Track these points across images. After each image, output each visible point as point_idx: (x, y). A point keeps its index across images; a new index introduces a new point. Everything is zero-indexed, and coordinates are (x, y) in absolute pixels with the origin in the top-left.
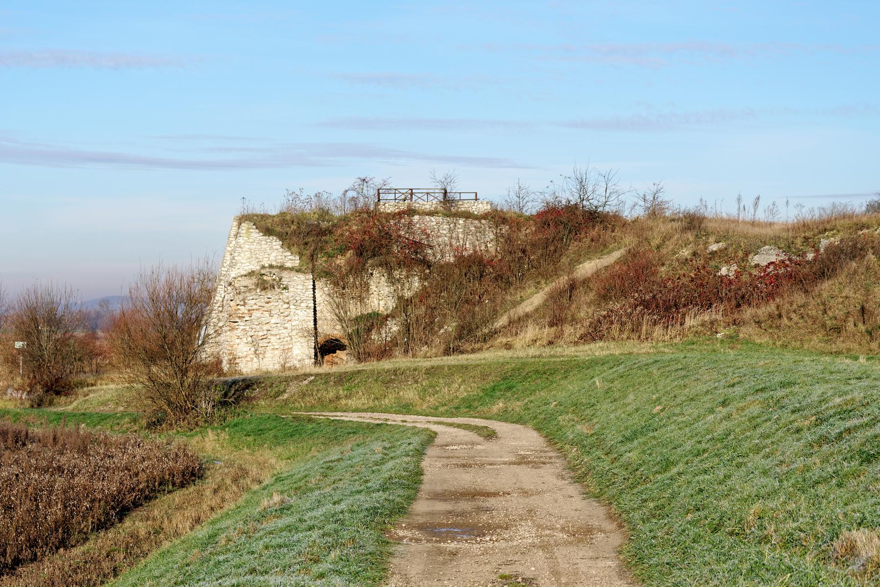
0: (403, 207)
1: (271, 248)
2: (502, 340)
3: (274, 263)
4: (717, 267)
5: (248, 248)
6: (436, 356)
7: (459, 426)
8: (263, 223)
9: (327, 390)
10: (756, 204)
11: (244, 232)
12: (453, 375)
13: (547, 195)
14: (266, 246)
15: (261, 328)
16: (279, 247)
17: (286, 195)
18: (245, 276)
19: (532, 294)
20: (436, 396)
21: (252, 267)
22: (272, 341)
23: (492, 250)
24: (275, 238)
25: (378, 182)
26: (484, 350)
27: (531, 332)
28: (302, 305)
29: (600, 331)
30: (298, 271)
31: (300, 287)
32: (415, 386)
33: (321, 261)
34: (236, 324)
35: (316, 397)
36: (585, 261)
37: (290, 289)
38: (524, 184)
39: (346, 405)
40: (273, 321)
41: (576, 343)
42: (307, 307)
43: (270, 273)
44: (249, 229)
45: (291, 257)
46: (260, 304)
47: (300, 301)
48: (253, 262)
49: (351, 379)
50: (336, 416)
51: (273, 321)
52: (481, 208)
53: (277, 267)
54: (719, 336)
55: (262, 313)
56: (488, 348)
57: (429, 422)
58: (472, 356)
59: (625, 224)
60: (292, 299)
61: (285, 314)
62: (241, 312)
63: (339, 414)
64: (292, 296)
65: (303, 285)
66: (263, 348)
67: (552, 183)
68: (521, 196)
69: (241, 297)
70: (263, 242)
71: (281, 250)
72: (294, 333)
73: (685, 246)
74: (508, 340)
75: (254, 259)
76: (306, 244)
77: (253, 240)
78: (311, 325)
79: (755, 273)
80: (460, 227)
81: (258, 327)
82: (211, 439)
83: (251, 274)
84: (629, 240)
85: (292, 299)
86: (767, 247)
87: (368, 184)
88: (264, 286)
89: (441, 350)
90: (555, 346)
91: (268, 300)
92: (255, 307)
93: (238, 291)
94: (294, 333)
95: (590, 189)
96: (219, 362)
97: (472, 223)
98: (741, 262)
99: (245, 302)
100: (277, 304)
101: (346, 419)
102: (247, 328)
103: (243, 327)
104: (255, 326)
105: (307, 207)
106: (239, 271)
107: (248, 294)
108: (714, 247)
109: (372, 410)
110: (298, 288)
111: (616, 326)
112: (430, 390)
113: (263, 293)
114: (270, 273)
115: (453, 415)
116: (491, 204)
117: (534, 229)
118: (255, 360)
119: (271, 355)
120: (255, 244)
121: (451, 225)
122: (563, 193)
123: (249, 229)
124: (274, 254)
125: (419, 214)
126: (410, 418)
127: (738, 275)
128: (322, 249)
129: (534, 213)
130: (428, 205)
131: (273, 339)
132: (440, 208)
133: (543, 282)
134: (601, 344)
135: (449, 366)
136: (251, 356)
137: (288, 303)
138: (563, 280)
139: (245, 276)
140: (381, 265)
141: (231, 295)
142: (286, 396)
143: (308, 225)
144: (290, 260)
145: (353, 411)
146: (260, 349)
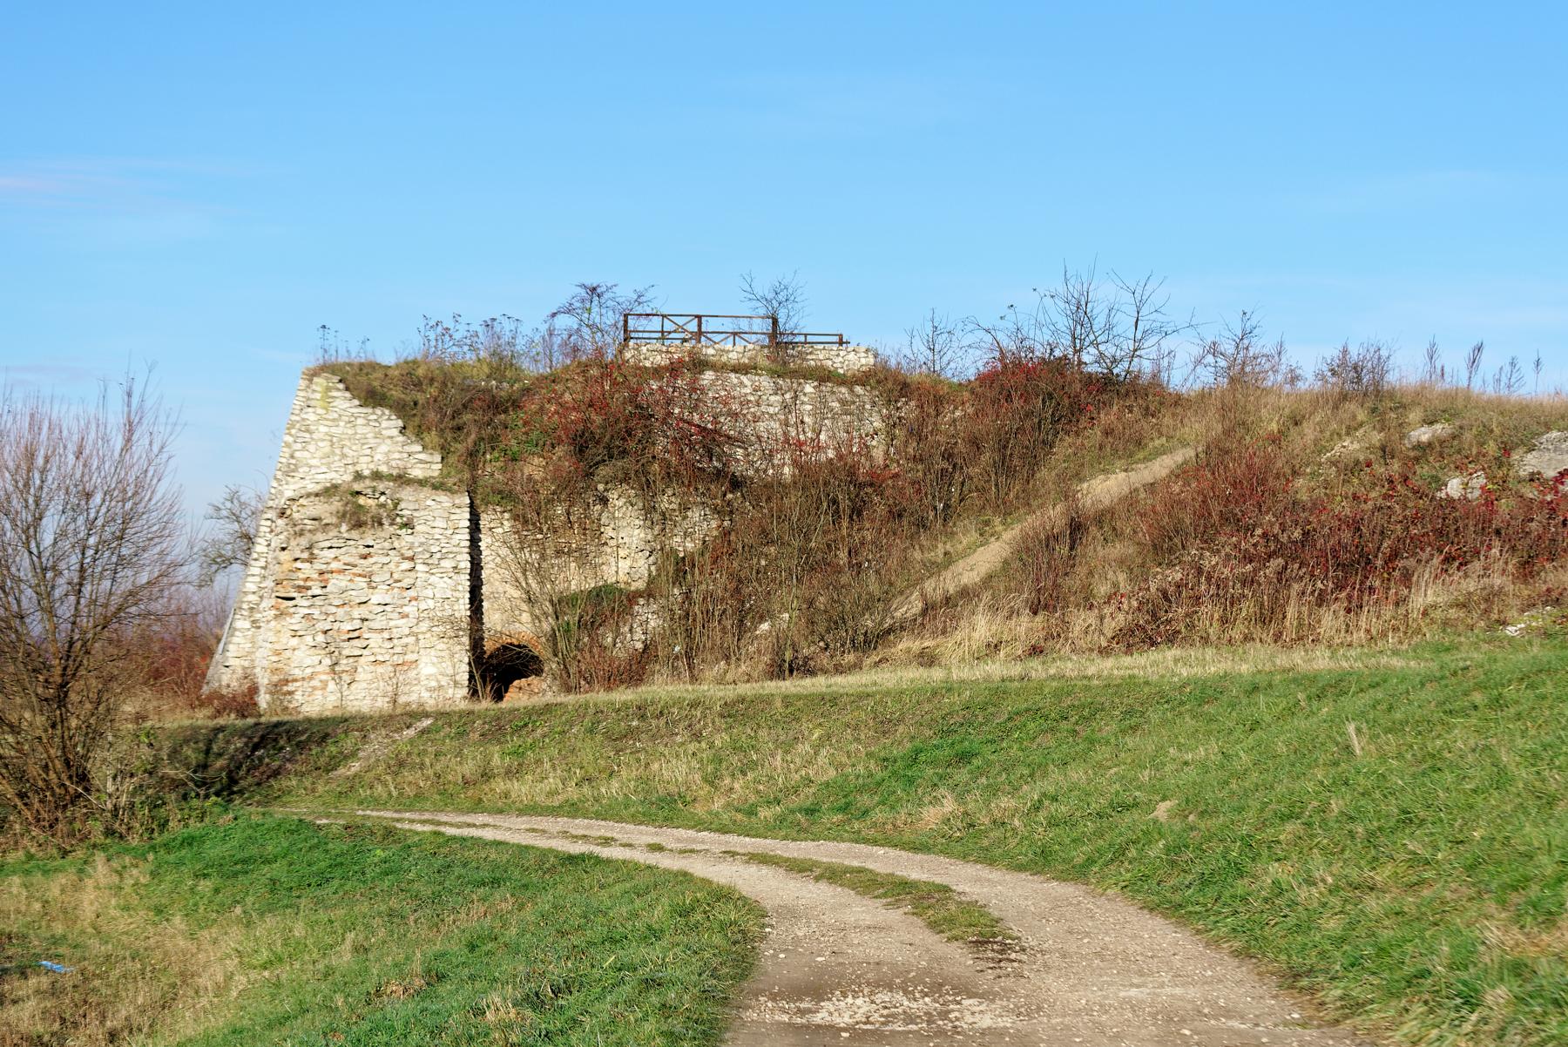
0: (679, 351)
1: (378, 435)
2: (907, 644)
3: (384, 469)
4: (1436, 479)
5: (326, 434)
6: (748, 681)
7: (833, 875)
8: (363, 379)
9: (460, 754)
10: (1474, 362)
11: (318, 396)
12: (798, 720)
13: (1001, 337)
14: (366, 430)
15: (347, 613)
16: (395, 432)
17: (422, 329)
18: (317, 495)
19: (971, 549)
20: (750, 776)
21: (333, 475)
22: (372, 643)
23: (878, 454)
24: (387, 412)
25: (624, 293)
26: (865, 669)
27: (981, 627)
28: (444, 563)
29: (1169, 622)
30: (438, 486)
31: (440, 523)
32: (692, 747)
33: (492, 470)
34: (291, 603)
35: (430, 772)
36: (1093, 476)
37: (418, 528)
38: (944, 320)
39: (507, 795)
40: (376, 598)
41: (1104, 652)
42: (455, 568)
43: (374, 489)
44: (328, 389)
45: (422, 456)
46: (347, 559)
47: (438, 555)
48: (336, 464)
49: (526, 725)
50: (469, 825)
51: (376, 598)
52: (853, 361)
53: (390, 478)
54: (1511, 630)
55: (351, 580)
56: (877, 664)
57: (733, 854)
58: (839, 679)
59: (1178, 401)
60: (420, 549)
61: (405, 584)
62: (301, 576)
63: (480, 819)
64: (422, 544)
65: (448, 519)
66: (351, 660)
67: (1011, 311)
68: (937, 348)
69: (304, 542)
70: (360, 421)
71: (401, 438)
72: (424, 626)
73: (1348, 434)
74: (926, 644)
75: (337, 458)
76: (459, 428)
77: (336, 416)
78: (463, 608)
79: (1531, 496)
80: (806, 399)
81: (341, 611)
82: (103, 881)
83: (330, 491)
84: (1198, 430)
85: (420, 549)
86: (1555, 434)
87: (602, 301)
88: (357, 519)
89: (761, 667)
90: (1050, 658)
91: (367, 550)
92: (334, 566)
93: (297, 529)
94: (424, 626)
95: (1099, 323)
96: (254, 690)
97: (833, 393)
98: (1495, 468)
99: (312, 554)
100: (386, 560)
101: (488, 834)
102: (316, 612)
103: (307, 611)
104: (334, 610)
105: (466, 356)
106: (303, 483)
107: (320, 536)
108: (1423, 434)
109: (573, 809)
110: (435, 525)
111: (1209, 612)
112: (735, 760)
113: (355, 534)
114: (374, 489)
115: (802, 833)
116: (876, 356)
117: (970, 411)
118: (332, 686)
119: (370, 676)
120: (342, 424)
121: (788, 396)
122: (1038, 332)
123: (328, 389)
124: (384, 448)
125: (713, 367)
126: (672, 837)
127: (1490, 500)
128: (493, 441)
129: (971, 374)
130: (735, 352)
131: (375, 640)
132: (762, 361)
133: (997, 520)
134: (1174, 652)
135: (786, 697)
136: (324, 677)
137: (412, 559)
138: (1055, 515)
139: (317, 495)
140: (625, 479)
141: (282, 537)
142: (355, 767)
143: (464, 389)
144: (421, 462)
145: (521, 812)
146: (345, 661)
